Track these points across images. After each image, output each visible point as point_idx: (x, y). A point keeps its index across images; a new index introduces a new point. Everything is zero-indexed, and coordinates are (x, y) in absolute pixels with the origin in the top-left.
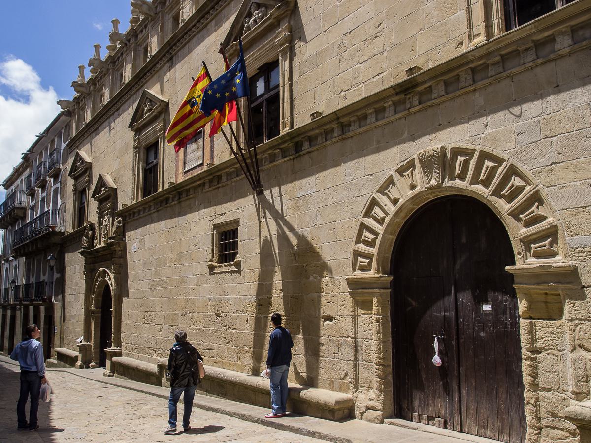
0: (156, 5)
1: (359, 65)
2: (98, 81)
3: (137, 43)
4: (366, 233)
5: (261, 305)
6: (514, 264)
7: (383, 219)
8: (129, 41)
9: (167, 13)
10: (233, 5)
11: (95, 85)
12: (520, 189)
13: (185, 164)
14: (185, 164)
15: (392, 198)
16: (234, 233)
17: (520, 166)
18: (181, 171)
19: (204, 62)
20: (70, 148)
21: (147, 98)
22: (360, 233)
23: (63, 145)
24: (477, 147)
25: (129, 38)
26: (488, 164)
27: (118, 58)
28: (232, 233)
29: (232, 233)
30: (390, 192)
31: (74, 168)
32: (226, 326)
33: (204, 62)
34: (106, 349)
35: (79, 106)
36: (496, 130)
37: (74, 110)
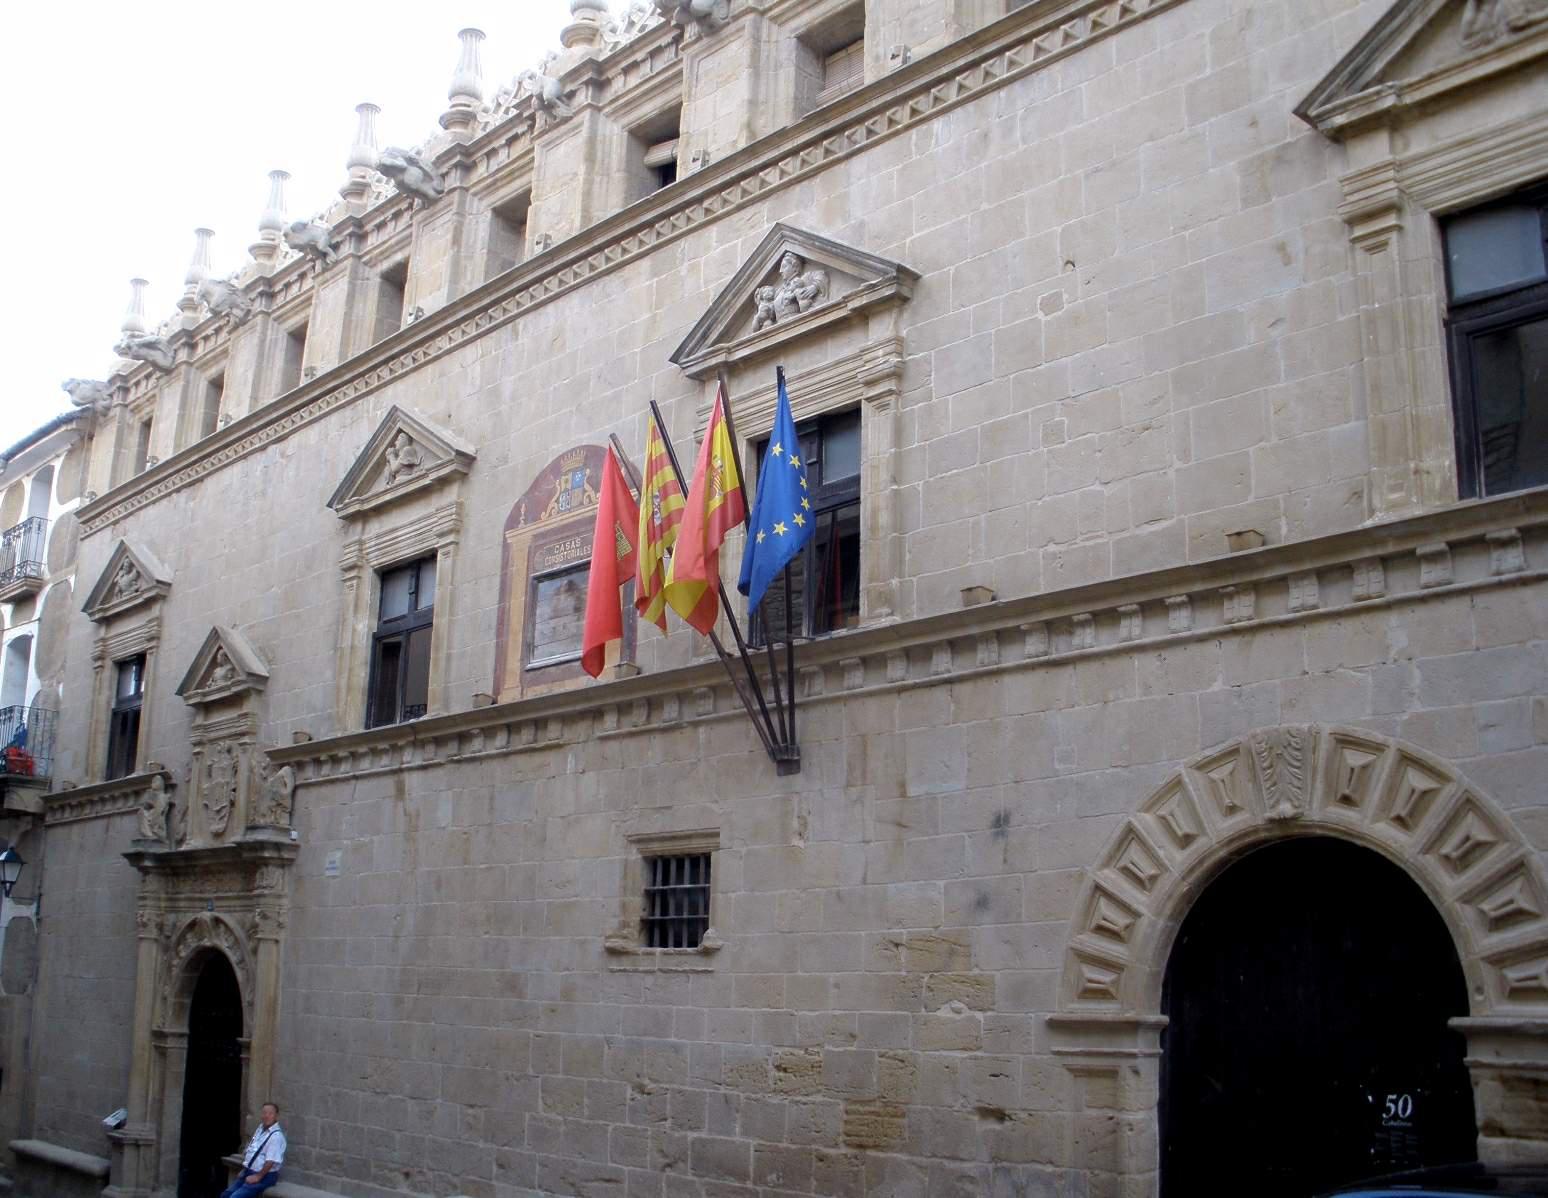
0: (444, 170)
1: (1097, 487)
2: (206, 338)
3: (360, 257)
4: (1105, 908)
5: (785, 1070)
6: (1464, 1011)
7: (1153, 878)
8: (335, 247)
9: (475, 194)
10: (714, 234)
11: (193, 347)
12: (1481, 846)
13: (529, 648)
14: (529, 648)
15: (1180, 833)
16: (700, 863)
17: (1484, 795)
18: (514, 664)
19: (653, 404)
20: (84, 523)
21: (400, 431)
22: (1089, 908)
23: (58, 510)
24: (1391, 741)
25: (338, 239)
26: (1417, 781)
27: (288, 286)
28: (660, 864)
29: (660, 864)
30: (1173, 815)
31: (104, 589)
32: (665, 1120)
33: (653, 404)
34: (228, 1155)
35: (124, 399)
36: (950, 835)
37: (108, 409)
